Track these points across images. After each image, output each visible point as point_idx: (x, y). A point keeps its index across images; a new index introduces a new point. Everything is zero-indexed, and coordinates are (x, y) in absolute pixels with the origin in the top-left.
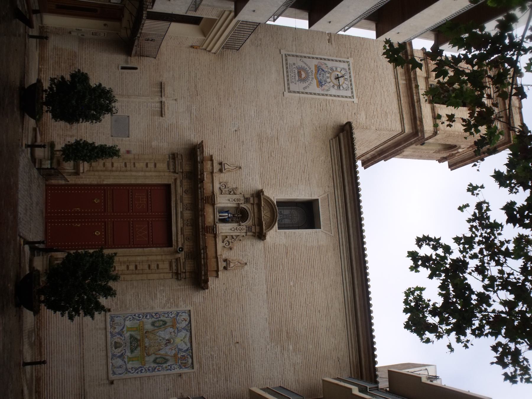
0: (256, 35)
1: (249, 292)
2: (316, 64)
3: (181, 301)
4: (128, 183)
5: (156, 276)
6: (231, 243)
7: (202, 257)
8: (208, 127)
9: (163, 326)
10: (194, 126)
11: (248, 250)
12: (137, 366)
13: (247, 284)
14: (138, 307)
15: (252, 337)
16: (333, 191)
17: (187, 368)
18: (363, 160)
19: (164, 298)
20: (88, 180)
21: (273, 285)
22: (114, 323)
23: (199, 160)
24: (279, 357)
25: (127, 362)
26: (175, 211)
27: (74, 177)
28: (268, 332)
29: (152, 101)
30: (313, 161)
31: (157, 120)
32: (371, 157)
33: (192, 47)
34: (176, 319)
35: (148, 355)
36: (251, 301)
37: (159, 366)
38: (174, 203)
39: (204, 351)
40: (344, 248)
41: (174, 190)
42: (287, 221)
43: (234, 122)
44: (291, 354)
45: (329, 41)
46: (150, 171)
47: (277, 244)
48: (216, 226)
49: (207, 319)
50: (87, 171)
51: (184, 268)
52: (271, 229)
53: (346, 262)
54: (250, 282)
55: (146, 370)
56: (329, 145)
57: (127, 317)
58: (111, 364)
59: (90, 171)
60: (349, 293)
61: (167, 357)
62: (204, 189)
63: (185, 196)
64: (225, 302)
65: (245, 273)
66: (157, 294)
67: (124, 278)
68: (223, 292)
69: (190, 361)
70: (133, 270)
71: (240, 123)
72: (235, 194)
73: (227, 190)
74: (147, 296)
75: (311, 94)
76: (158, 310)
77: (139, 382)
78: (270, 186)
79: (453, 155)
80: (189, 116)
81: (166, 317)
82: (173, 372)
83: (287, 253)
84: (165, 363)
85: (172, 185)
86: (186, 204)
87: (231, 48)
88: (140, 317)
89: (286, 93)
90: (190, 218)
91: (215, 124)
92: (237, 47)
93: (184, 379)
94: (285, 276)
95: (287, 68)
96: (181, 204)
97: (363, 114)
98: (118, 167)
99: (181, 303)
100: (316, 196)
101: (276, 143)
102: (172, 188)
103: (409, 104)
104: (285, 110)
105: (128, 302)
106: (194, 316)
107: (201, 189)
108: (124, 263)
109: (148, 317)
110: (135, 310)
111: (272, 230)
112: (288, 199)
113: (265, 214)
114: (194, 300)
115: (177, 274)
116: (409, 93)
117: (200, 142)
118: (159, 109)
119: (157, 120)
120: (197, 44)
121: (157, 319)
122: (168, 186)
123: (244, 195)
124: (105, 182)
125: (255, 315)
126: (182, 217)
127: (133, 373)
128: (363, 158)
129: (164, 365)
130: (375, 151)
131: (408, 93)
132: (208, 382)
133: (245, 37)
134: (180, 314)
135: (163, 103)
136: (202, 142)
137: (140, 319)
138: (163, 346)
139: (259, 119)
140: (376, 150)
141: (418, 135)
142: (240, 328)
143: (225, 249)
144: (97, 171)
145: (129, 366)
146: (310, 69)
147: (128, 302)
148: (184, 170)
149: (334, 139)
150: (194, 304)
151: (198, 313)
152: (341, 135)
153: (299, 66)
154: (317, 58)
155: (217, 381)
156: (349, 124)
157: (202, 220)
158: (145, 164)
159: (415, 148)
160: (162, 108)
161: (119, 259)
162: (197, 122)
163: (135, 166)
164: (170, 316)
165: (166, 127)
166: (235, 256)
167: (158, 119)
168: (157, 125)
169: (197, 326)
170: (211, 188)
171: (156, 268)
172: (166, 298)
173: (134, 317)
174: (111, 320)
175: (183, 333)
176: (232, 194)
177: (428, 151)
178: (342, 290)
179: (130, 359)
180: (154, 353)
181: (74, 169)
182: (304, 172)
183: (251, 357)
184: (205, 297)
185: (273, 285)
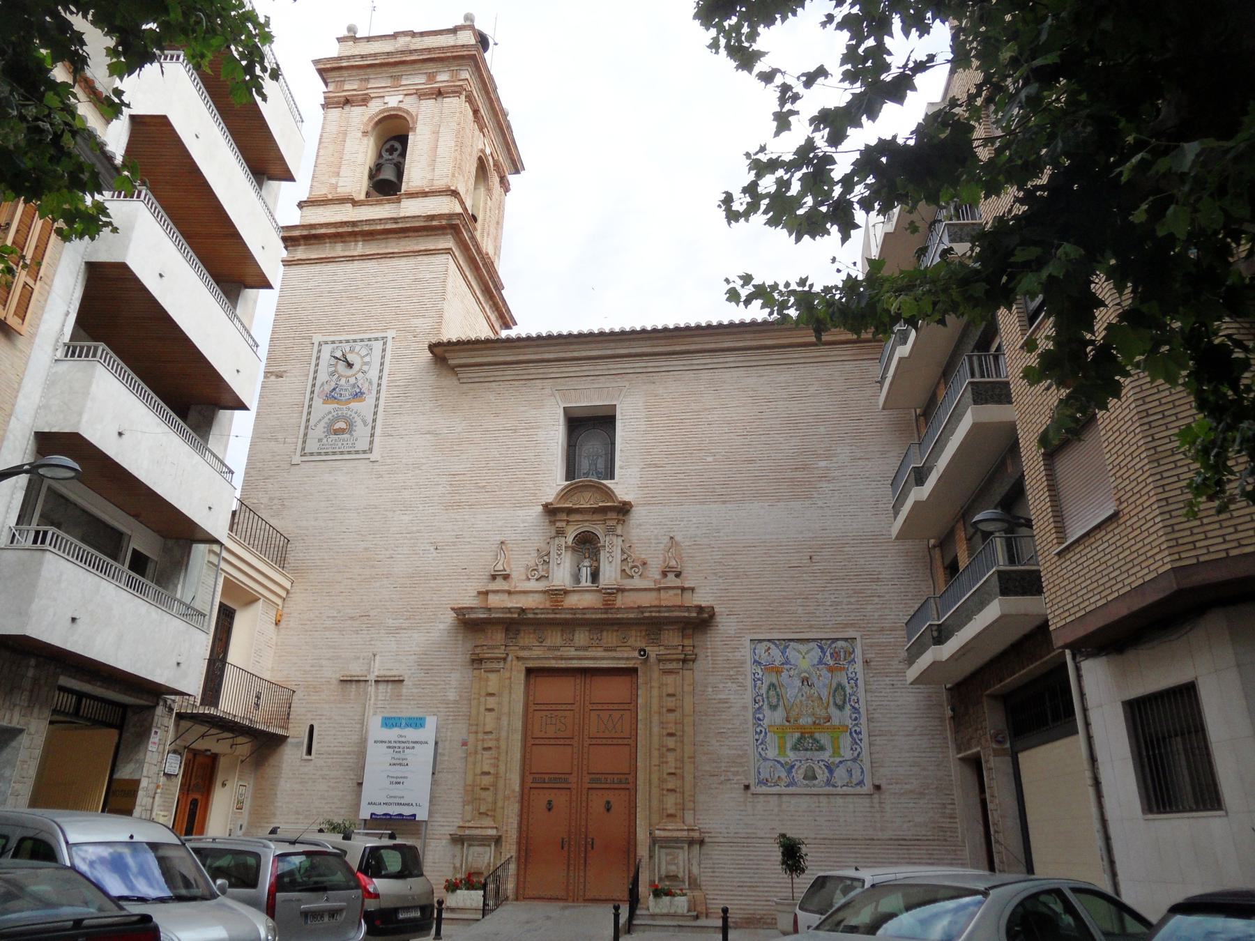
0: (262, 506)
1: (721, 534)
2: (322, 400)
4: (519, 744)
6: (636, 564)
7: (657, 614)
9: (778, 690)
12: (849, 739)
14: (742, 735)
15: (801, 532)
16: (551, 380)
17: (854, 651)
18: (501, 326)
20: (510, 820)
23: (485, 616)
24: (841, 484)
25: (841, 759)
29: (373, 699)
30: (497, 415)
31: (410, 691)
32: (496, 313)
33: (277, 623)
35: (829, 719)
37: (850, 701)
38: (560, 662)
39: (825, 619)
40: (652, 364)
41: (536, 662)
42: (601, 465)
43: (421, 552)
44: (834, 465)
45: (279, 375)
46: (499, 703)
49: (767, 610)
51: (676, 647)
52: (613, 492)
53: (676, 363)
54: (704, 532)
55: (856, 725)
56: (471, 385)
57: (760, 754)
58: (845, 788)
59: (494, 816)
60: (731, 358)
61: (834, 685)
62: (537, 608)
63: (548, 643)
68: (720, 581)
69: (840, 644)
70: (676, 742)
71: (422, 541)
74: (723, 717)
75: (375, 413)
76: (748, 697)
77: (878, 738)
78: (537, 492)
79: (496, 164)
80: (405, 631)
82: (860, 676)
83: (656, 466)
84: (843, 689)
85: (529, 666)
87: (284, 552)
88: (761, 731)
89: (373, 457)
90: (587, 634)
92: (282, 543)
93: (873, 656)
95: (327, 454)
97: (416, 322)
99: (738, 655)
100: (558, 412)
101: (461, 477)
103: (400, 238)
104: (404, 461)
105: (734, 752)
106: (762, 633)
107: (537, 614)
108: (662, 756)
109: (761, 716)
110: (747, 739)
111: (614, 490)
112: (562, 460)
113: (586, 501)
115: (684, 661)
116: (379, 237)
117: (452, 612)
118: (390, 686)
119: (410, 691)
120: (273, 614)
122: (529, 671)
124: (517, 788)
126: (585, 649)
127: (861, 748)
128: (497, 326)
129: (848, 691)
130: (484, 305)
131: (380, 239)
132: (880, 613)
133: (263, 527)
134: (757, 658)
135: (379, 679)
136: (453, 609)
137: (763, 730)
138: (812, 691)
140: (483, 302)
141: (457, 225)
145: (848, 754)
146: (330, 413)
147: (734, 752)
149: (460, 376)
150: (740, 633)
152: (450, 362)
153: (324, 432)
154: (311, 399)
155: (879, 596)
156: (433, 347)
157: (592, 613)
159: (482, 233)
160: (388, 681)
161: (655, 766)
163: (491, 732)
164: (760, 676)
165: (423, 675)
170: (536, 595)
171: (674, 699)
174: (765, 784)
175: (790, 653)
177: (488, 210)
178: (725, 370)
179: (836, 752)
180: (826, 709)
181: (489, 846)
183: (838, 535)
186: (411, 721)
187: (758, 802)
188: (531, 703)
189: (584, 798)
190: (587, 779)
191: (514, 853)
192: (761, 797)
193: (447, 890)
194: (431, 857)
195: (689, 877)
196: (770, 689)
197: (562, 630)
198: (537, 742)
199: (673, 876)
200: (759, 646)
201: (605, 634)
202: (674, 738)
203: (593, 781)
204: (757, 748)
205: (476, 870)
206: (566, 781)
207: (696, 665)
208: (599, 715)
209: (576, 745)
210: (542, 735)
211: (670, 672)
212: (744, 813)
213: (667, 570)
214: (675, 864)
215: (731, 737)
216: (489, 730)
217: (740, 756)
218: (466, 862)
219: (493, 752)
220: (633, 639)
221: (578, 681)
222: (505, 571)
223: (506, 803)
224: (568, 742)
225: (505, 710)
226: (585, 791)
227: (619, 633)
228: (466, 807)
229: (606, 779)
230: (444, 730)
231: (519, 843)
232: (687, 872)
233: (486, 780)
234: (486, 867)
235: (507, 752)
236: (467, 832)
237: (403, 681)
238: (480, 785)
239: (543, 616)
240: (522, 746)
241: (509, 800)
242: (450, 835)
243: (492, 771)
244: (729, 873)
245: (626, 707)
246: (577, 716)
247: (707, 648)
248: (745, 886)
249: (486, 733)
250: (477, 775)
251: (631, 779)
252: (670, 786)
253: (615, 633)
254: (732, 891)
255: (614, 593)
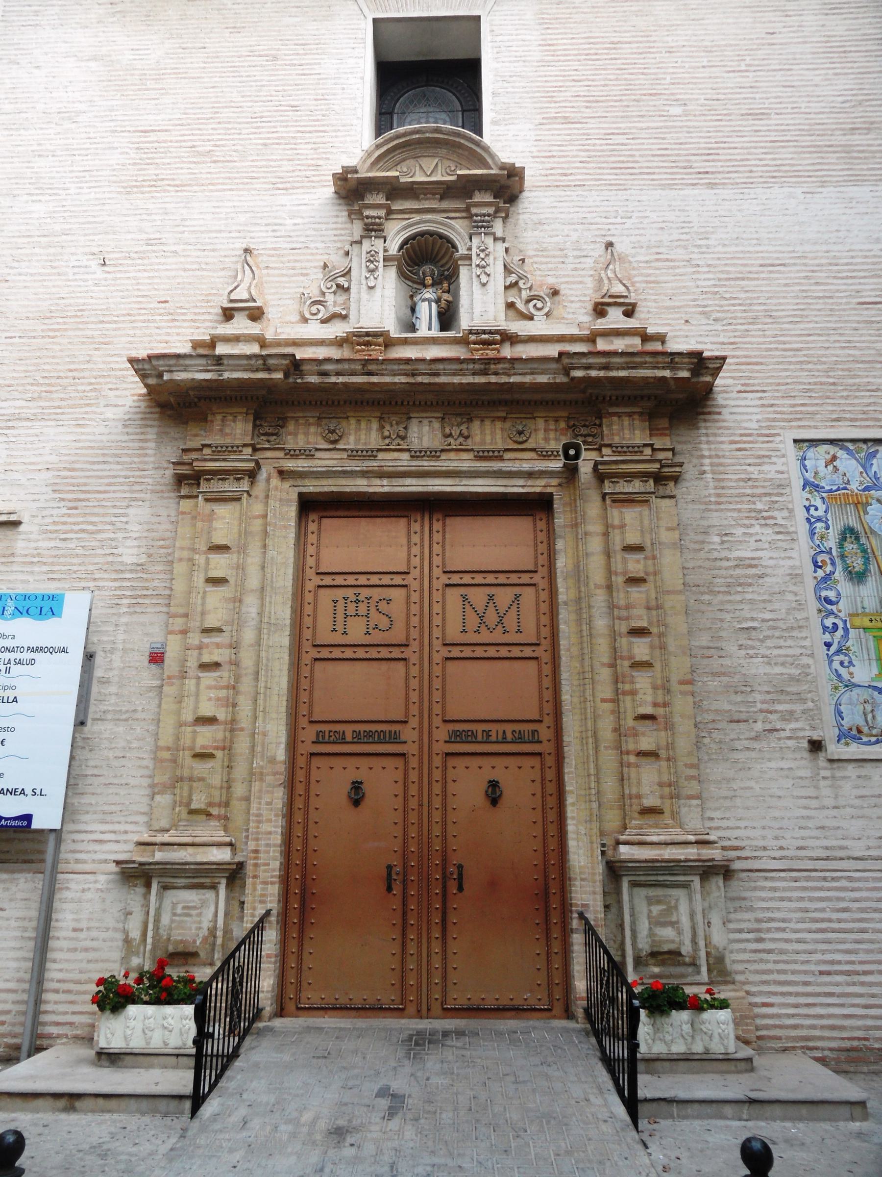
3: (760, 472)
4: (286, 657)
5: (669, 561)
7: (602, 374)
8: (81, 359)
9: (863, 540)
10: (70, 407)
11: (559, 239)
13: (685, 248)
19: (751, 531)
21: (685, 168)
22: (865, 730)
23: (208, 376)
26: (408, 481)
27: (248, 890)
28: (856, 188)
31: (33, 545)
34: (831, 491)
36: (745, 236)
38: (377, 482)
41: (324, 482)
46: (240, 568)
47: (534, 149)
48: (471, 332)
49: (821, 384)
50: (226, 829)
51: (637, 449)
54: (676, 236)
57: (839, 676)
59: (226, 818)
63: (350, 442)
64: (754, 321)
65: (643, 251)
66: (741, 559)
67: (681, 683)
70: (652, 647)
71: (73, 250)
72: (347, 273)
73: (330, 298)
74: (749, 596)
76: (803, 549)
80: (29, 424)
81: (827, 528)
83: (567, 121)
85: (304, 490)
86: (384, 438)
90: (437, 425)
91: (70, 333)
94: (648, 128)
96: (381, 456)
98: (218, 699)
99: (770, 471)
100: (363, 26)
101: (162, 136)
102: (318, 490)
105: (778, 670)
106: (816, 427)
109: (831, 595)
110: (807, 643)
114: (754, 425)
115: (659, 478)
119: (33, 545)
121: (838, 561)
123: (352, 243)
124: (281, 754)
125: (797, 228)
126: (433, 454)
134: (810, 476)
137: (841, 625)
139: (64, 189)
142: (847, 277)
143: (555, 313)
144: (228, 785)
147: (778, 670)
148: (248, 440)
151: (801, 412)
158: (210, 588)
161: (603, 700)
162: (55, 396)
163: (219, 630)
164: (820, 513)
165: (65, 511)
166: (581, 282)
167: (29, 540)
168: (52, 544)
169: (852, 420)
171: (640, 556)
172: (752, 525)
173: (833, 649)
174: (857, 739)
176: (350, 281)
181: (214, 887)
182: (275, 58)
184: (740, 388)
185: (685, 168)
186: (27, 604)
187: (844, 778)
188: (310, 573)
189: (437, 775)
190: (441, 733)
191: (273, 904)
192: (850, 767)
193: (102, 1008)
194: (69, 916)
195: (708, 954)
196: (844, 539)
197: (381, 418)
198: (325, 653)
199: (670, 952)
200: (811, 453)
201: (476, 424)
202: (646, 640)
203: (456, 737)
204: (831, 662)
205: (180, 948)
206: (394, 739)
207: (680, 491)
208: (464, 597)
209: (414, 659)
210: (338, 639)
211: (628, 500)
212: (814, 803)
213: (606, 300)
214: (672, 924)
215: (767, 637)
216: (216, 624)
217: (793, 679)
218: (157, 928)
219: (225, 674)
220: (541, 434)
221: (416, 527)
222: (255, 301)
223: (256, 786)
224: (396, 653)
225: (253, 582)
226: (437, 761)
227: (508, 424)
228: (158, 798)
229: (487, 733)
230: (111, 628)
231: (285, 880)
232: (702, 943)
233: (206, 737)
234: (205, 939)
235: (257, 673)
236: (159, 856)
237: (16, 524)
238: (192, 748)
239: (341, 379)
240: (291, 664)
241: (261, 780)
242: (118, 863)
243: (221, 715)
244: (799, 941)
245: (525, 578)
246: (415, 597)
247: (703, 457)
248: (838, 973)
249: (206, 631)
250: (185, 724)
251: (545, 733)
252: (646, 744)
253: (499, 424)
254: (806, 984)
255: (494, 343)
